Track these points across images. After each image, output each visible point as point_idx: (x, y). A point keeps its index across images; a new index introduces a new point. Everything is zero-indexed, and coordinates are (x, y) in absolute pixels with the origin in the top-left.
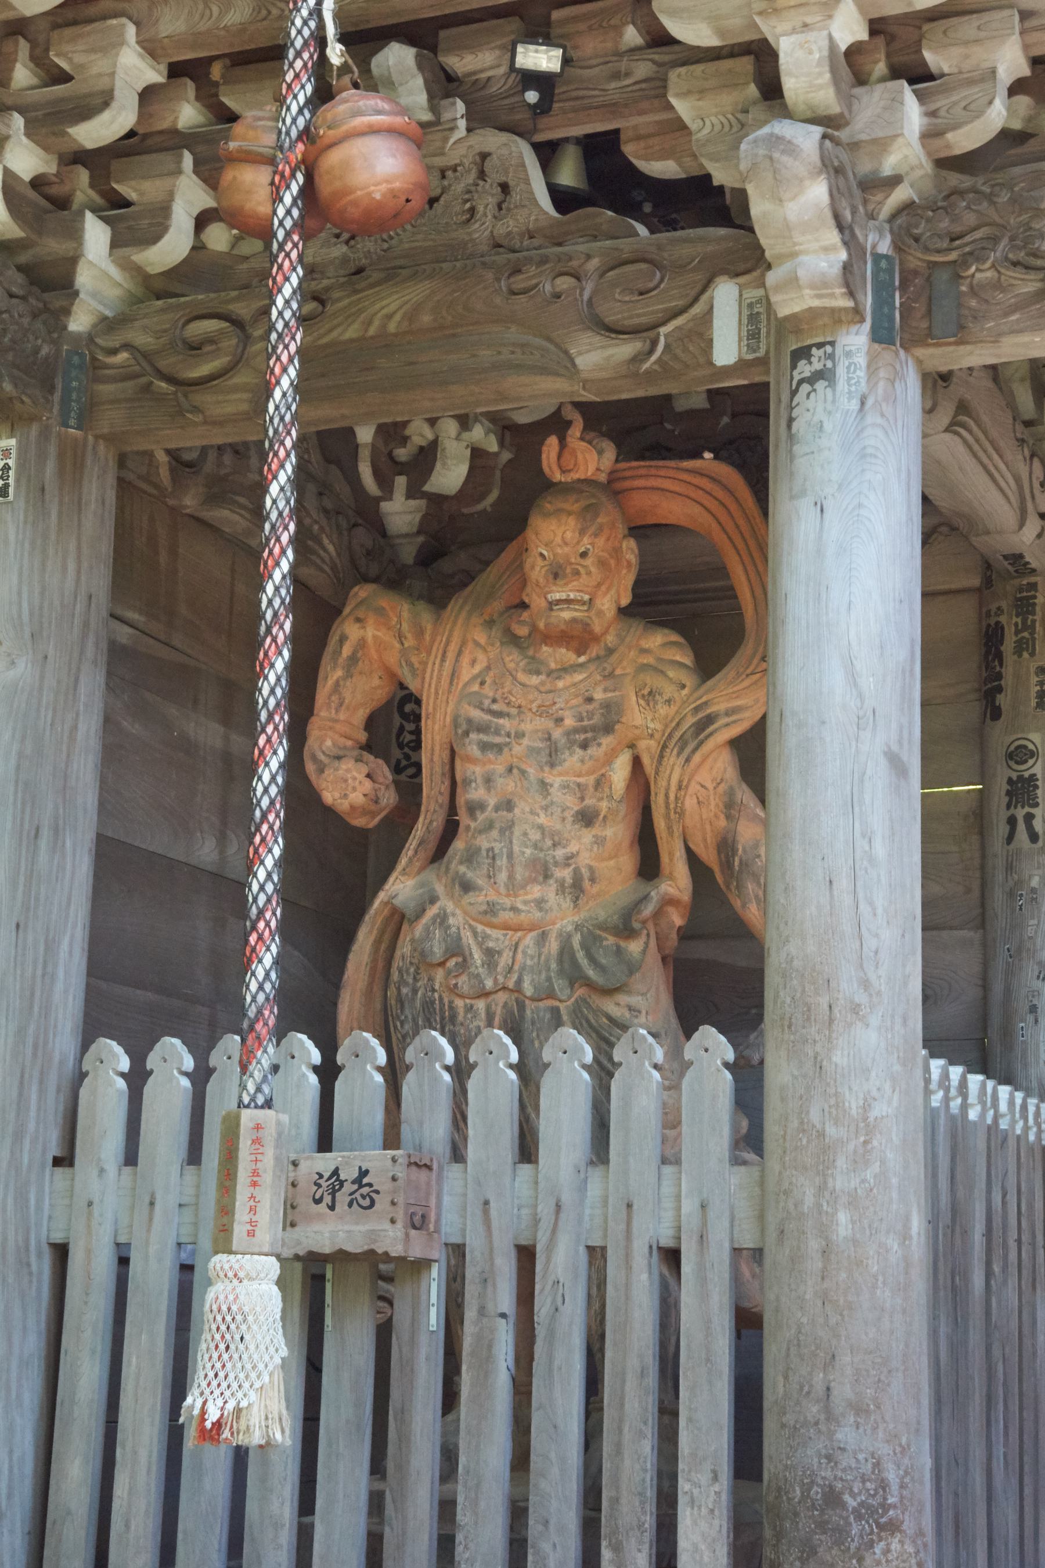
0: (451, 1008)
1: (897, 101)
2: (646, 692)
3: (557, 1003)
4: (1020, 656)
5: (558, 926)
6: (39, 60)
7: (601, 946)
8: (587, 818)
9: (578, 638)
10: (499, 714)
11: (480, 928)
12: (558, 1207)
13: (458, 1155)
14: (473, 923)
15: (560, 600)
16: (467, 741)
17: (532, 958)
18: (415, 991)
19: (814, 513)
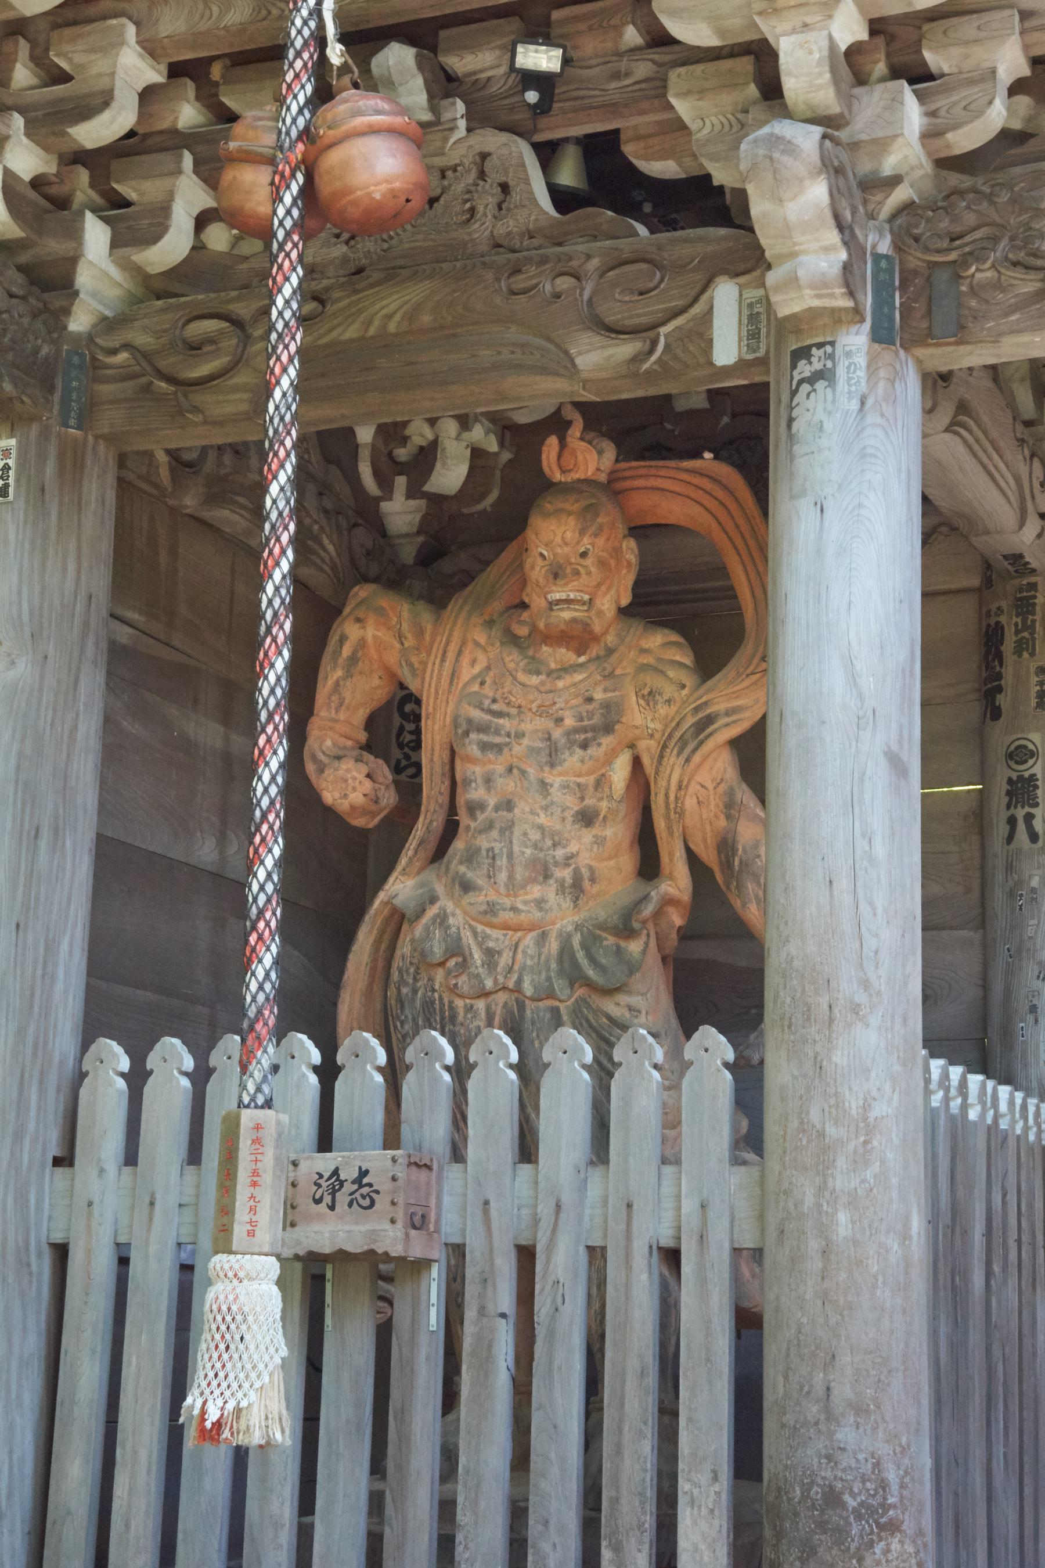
0: (451, 1008)
1: (897, 101)
2: (646, 692)
3: (557, 1003)
4: (1020, 656)
5: (558, 926)
6: (39, 60)
7: (601, 946)
8: (587, 818)
9: (578, 638)
10: (499, 714)
11: (480, 928)
12: (558, 1207)
13: (458, 1155)
14: (473, 923)
15: (560, 600)
16: (467, 741)
17: (532, 958)
18: (415, 991)
19: (814, 513)
